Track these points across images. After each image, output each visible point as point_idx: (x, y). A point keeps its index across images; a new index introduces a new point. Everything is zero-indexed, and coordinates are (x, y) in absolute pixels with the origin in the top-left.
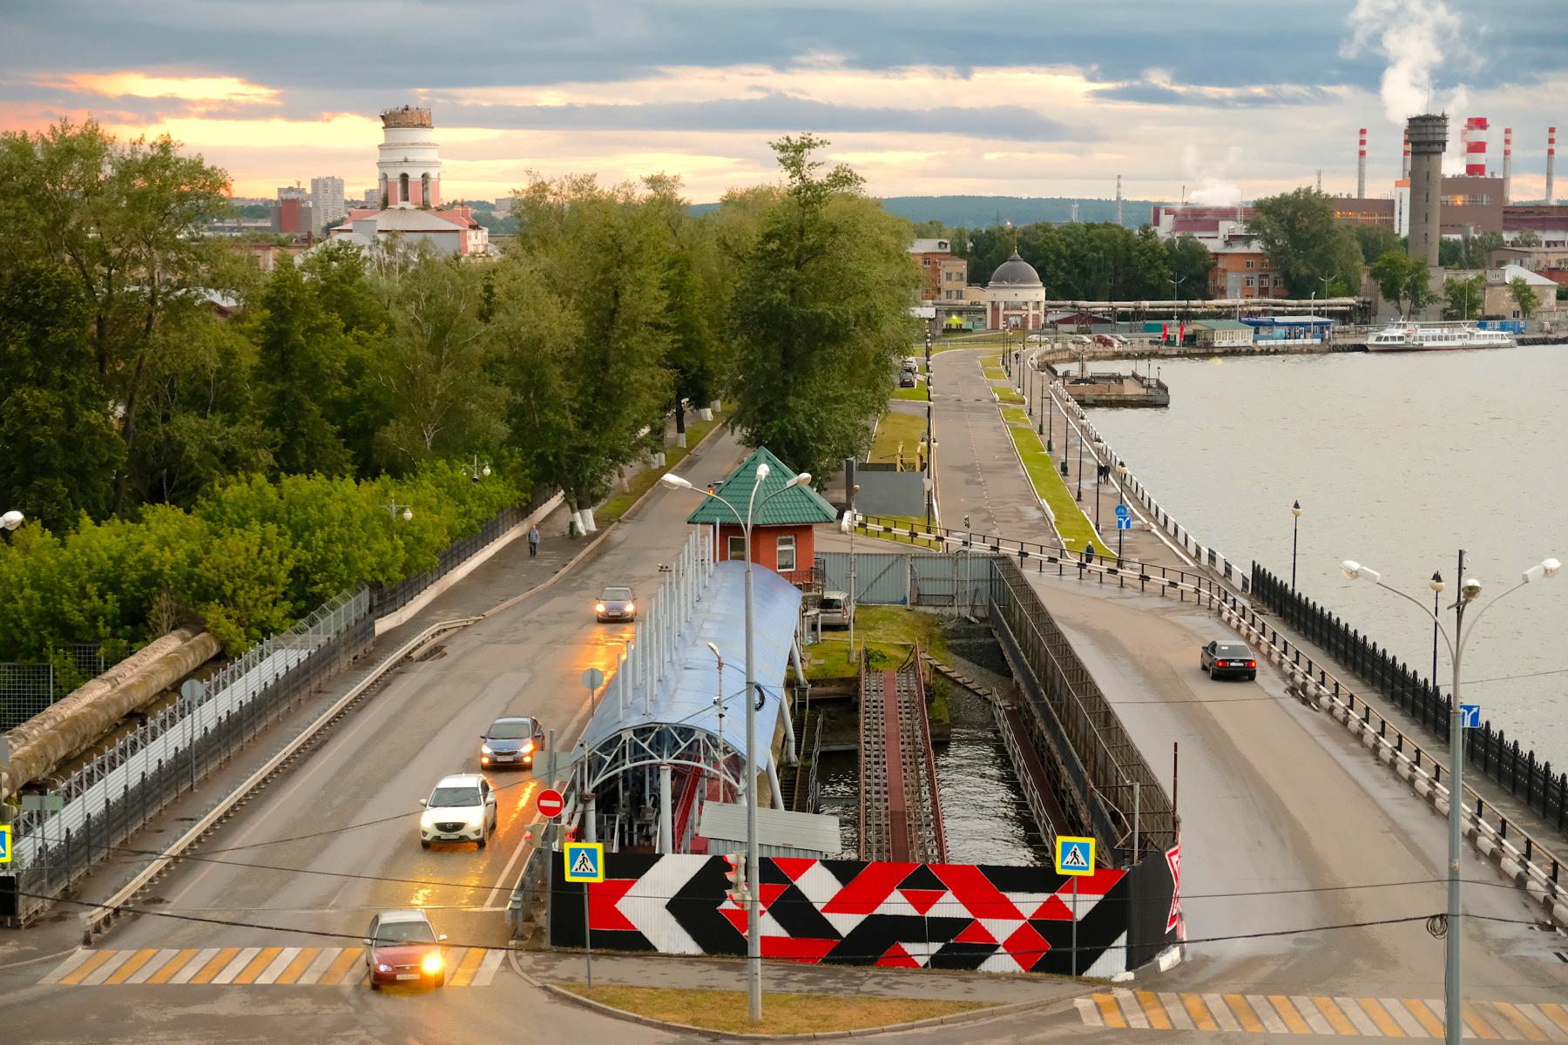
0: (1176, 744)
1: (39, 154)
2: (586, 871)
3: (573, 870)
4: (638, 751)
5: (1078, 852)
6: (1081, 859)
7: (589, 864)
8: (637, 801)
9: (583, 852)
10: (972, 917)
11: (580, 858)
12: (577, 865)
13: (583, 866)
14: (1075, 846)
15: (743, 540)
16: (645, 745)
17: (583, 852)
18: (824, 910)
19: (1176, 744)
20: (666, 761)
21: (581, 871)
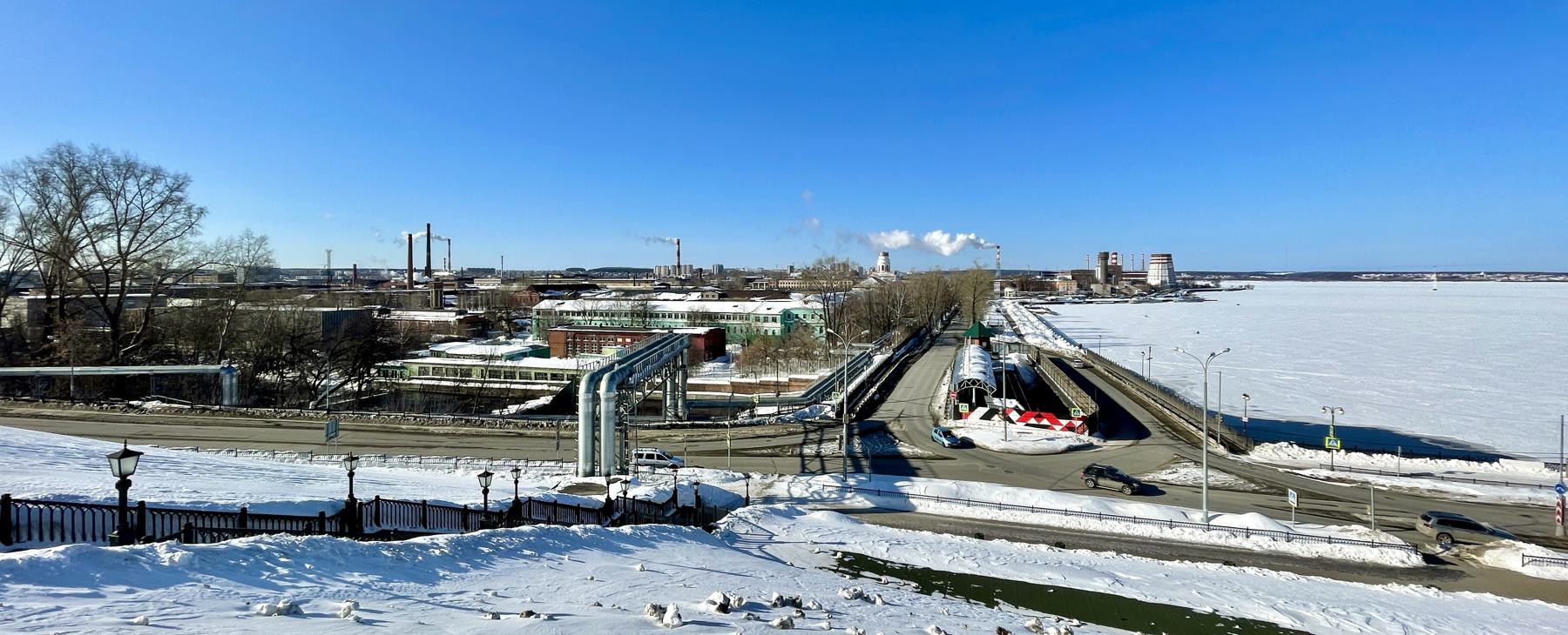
4: (968, 385)
20: (974, 387)
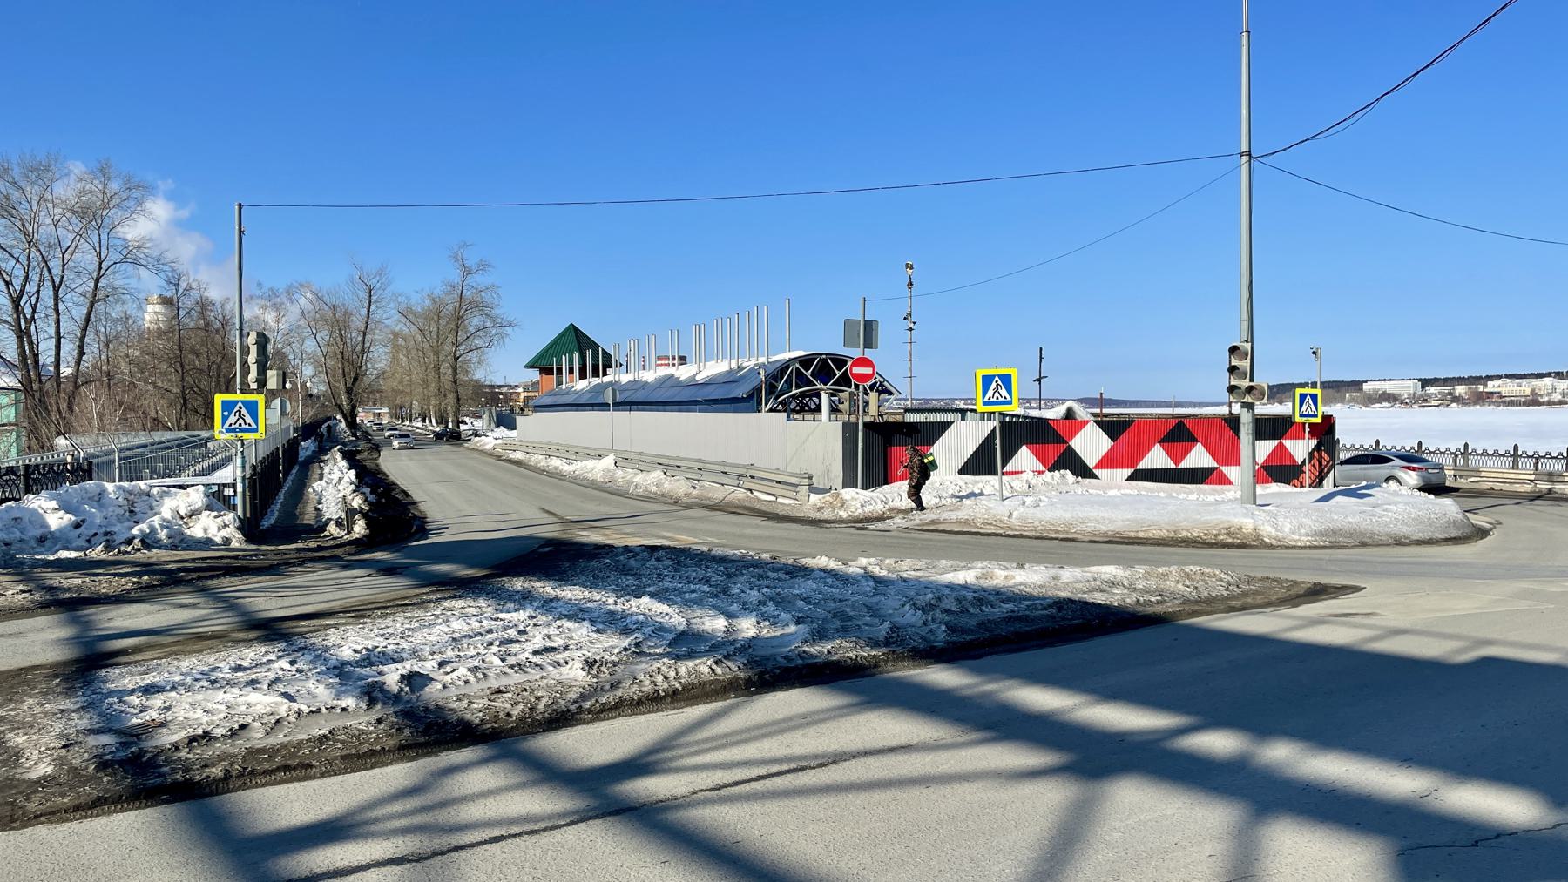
0: (1041, 349)
1: (308, 371)
2: (1000, 399)
3: (986, 399)
5: (244, 411)
6: (249, 419)
7: (1004, 392)
8: (131, 493)
9: (997, 378)
10: (1216, 465)
11: (994, 385)
12: (990, 393)
13: (997, 394)
14: (240, 404)
15: (785, 352)
16: (808, 374)
17: (997, 378)
18: (1095, 468)
19: (1041, 349)
21: (995, 399)
